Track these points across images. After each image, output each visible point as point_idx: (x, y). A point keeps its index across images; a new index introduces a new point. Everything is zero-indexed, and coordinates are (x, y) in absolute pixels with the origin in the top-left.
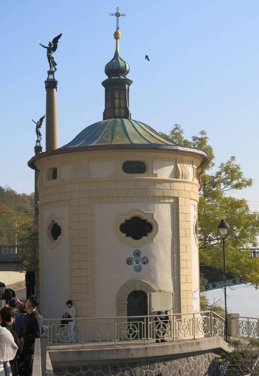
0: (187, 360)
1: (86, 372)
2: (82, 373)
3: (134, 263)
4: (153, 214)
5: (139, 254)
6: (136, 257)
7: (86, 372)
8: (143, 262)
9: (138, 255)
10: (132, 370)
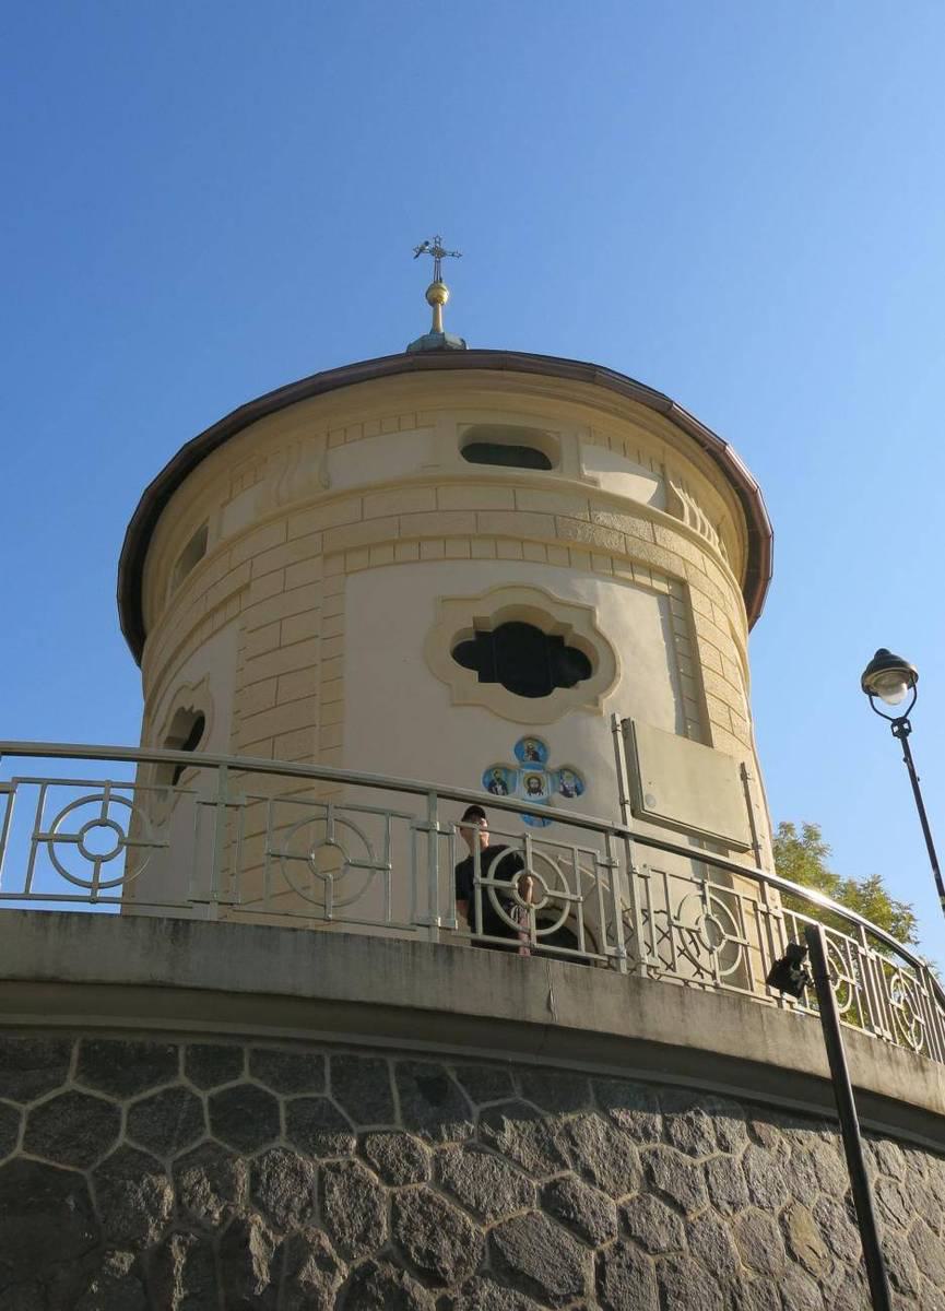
0: (877, 1154)
1: (215, 1090)
2: (180, 1093)
4: (590, 611)
5: (541, 753)
6: (528, 767)
7: (215, 1090)
8: (562, 789)
9: (536, 757)
10: (550, 1120)
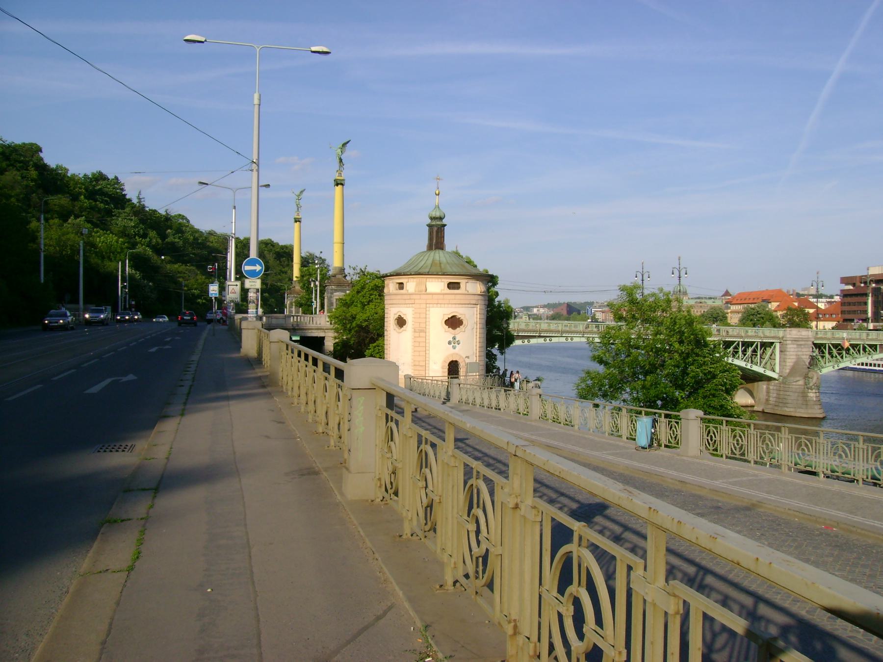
3: (453, 344)
